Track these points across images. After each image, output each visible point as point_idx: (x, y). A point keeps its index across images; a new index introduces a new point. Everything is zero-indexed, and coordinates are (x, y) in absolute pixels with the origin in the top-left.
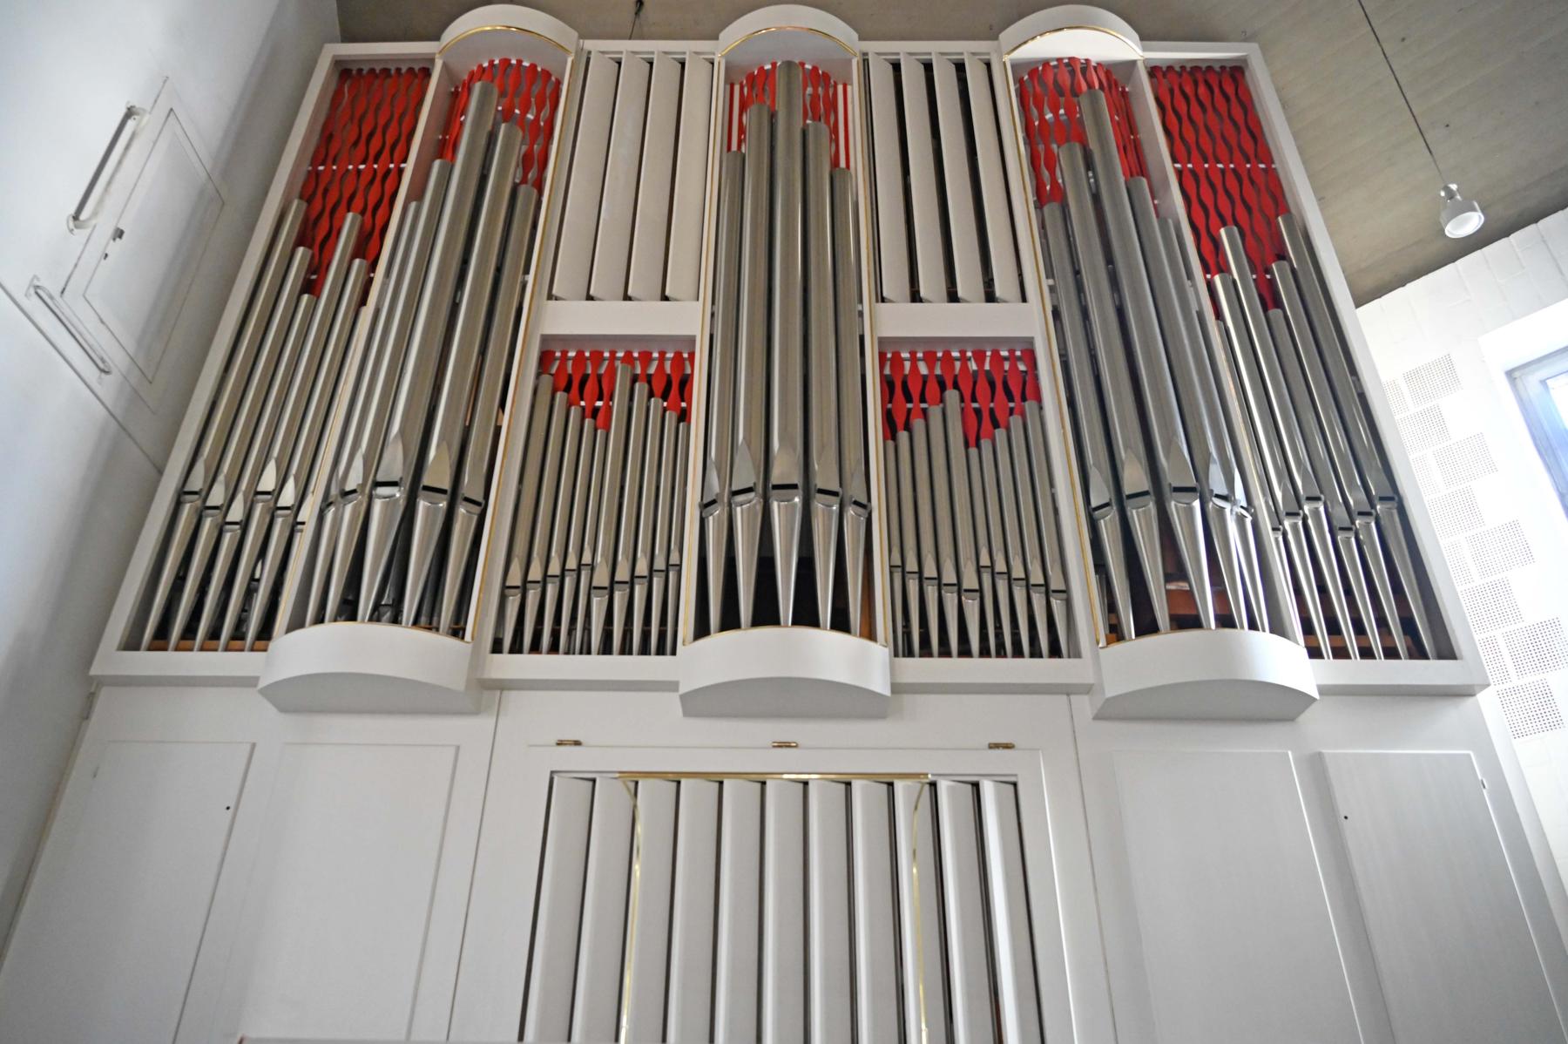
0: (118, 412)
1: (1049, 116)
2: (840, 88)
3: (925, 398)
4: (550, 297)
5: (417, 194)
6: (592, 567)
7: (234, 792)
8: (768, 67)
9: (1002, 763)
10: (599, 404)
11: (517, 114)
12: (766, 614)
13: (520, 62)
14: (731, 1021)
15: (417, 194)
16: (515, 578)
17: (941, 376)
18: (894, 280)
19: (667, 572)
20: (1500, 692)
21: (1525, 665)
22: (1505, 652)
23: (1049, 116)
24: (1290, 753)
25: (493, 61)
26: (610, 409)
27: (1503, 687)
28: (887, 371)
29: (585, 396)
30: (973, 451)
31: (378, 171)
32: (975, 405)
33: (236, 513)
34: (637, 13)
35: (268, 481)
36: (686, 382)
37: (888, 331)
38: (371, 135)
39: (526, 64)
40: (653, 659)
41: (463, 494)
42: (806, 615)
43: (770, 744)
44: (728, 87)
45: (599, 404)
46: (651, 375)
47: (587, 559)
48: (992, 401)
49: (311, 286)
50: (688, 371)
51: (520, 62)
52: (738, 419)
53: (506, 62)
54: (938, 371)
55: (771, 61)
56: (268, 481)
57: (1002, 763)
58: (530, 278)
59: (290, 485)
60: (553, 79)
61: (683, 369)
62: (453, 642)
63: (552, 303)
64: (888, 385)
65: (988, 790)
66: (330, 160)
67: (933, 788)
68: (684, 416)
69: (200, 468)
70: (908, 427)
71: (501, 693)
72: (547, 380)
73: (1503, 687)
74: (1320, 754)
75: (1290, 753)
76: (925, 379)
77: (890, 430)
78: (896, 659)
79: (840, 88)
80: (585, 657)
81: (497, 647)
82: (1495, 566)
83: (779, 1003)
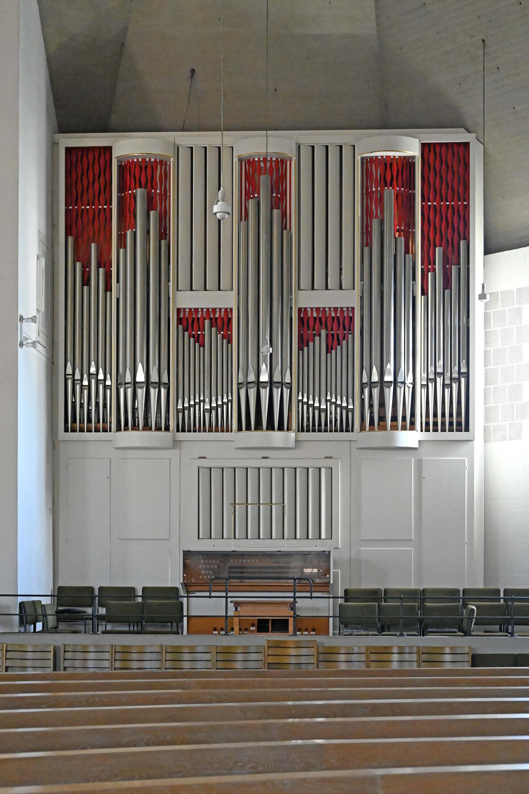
0: (47, 357)
1: (374, 189)
2: (288, 162)
5: (122, 243)
6: (204, 401)
7: (109, 473)
8: (257, 159)
9: (329, 463)
10: (199, 333)
11: (153, 192)
12: (258, 426)
14: (252, 530)
15: (122, 243)
22: (515, 410)
23: (374, 189)
24: (413, 459)
25: (139, 159)
26: (204, 335)
27: (511, 422)
30: (329, 355)
31: (95, 209)
32: (332, 332)
33: (85, 383)
34: (192, 77)
35: (93, 370)
36: (230, 320)
38: (82, 175)
40: (225, 434)
43: (261, 458)
44: (240, 162)
46: (217, 318)
49: (86, 281)
52: (249, 356)
53: (144, 160)
54: (320, 316)
56: (93, 370)
57: (329, 463)
58: (171, 284)
59: (101, 371)
60: (164, 162)
61: (228, 315)
62: (167, 433)
64: (301, 320)
65: (323, 471)
67: (189, 592)
68: (230, 341)
69: (69, 364)
70: (308, 346)
73: (511, 422)
74: (422, 459)
75: (413, 459)
76: (315, 318)
77: (300, 349)
79: (288, 162)
81: (178, 431)
83: (301, 510)
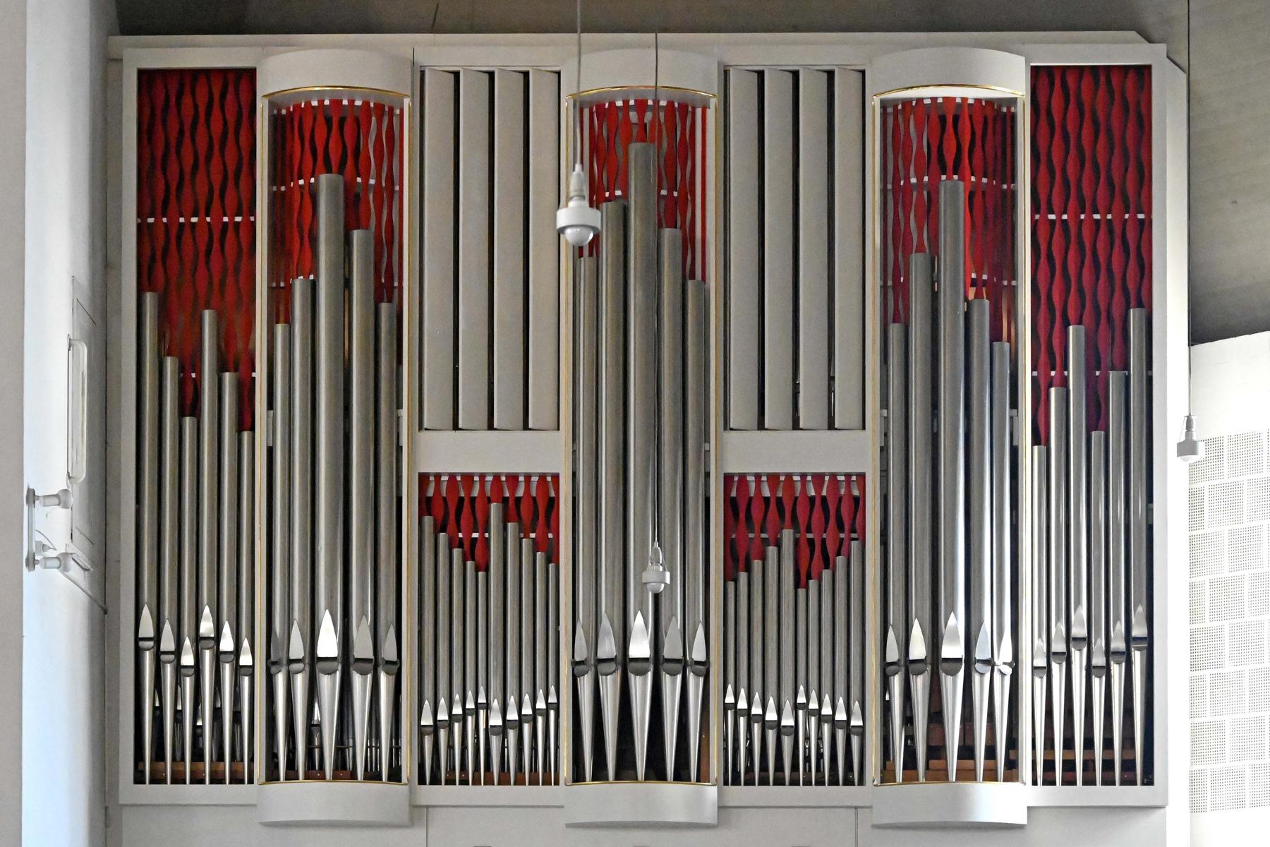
1: (914, 180)
2: (699, 112)
3: (765, 503)
4: (421, 427)
10: (475, 535)
12: (625, 770)
13: (352, 102)
16: (427, 720)
17: (780, 498)
18: (741, 409)
19: (547, 711)
20: (1212, 809)
21: (1198, 805)
23: (914, 180)
26: (487, 541)
28: (734, 494)
29: (462, 529)
30: (801, 592)
33: (188, 659)
35: (207, 627)
37: (734, 467)
39: (358, 103)
41: (383, 659)
42: (656, 771)
45: (475, 535)
47: (482, 700)
48: (825, 532)
50: (553, 494)
51: (352, 102)
53: (336, 103)
55: (625, 98)
56: (207, 627)
58: (404, 413)
60: (387, 109)
62: (394, 787)
63: (424, 434)
64: (731, 506)
66: (174, 231)
68: (553, 557)
71: (427, 811)
72: (428, 520)
78: (726, 787)
80: (489, 787)
81: (422, 781)
82: (1256, 683)
